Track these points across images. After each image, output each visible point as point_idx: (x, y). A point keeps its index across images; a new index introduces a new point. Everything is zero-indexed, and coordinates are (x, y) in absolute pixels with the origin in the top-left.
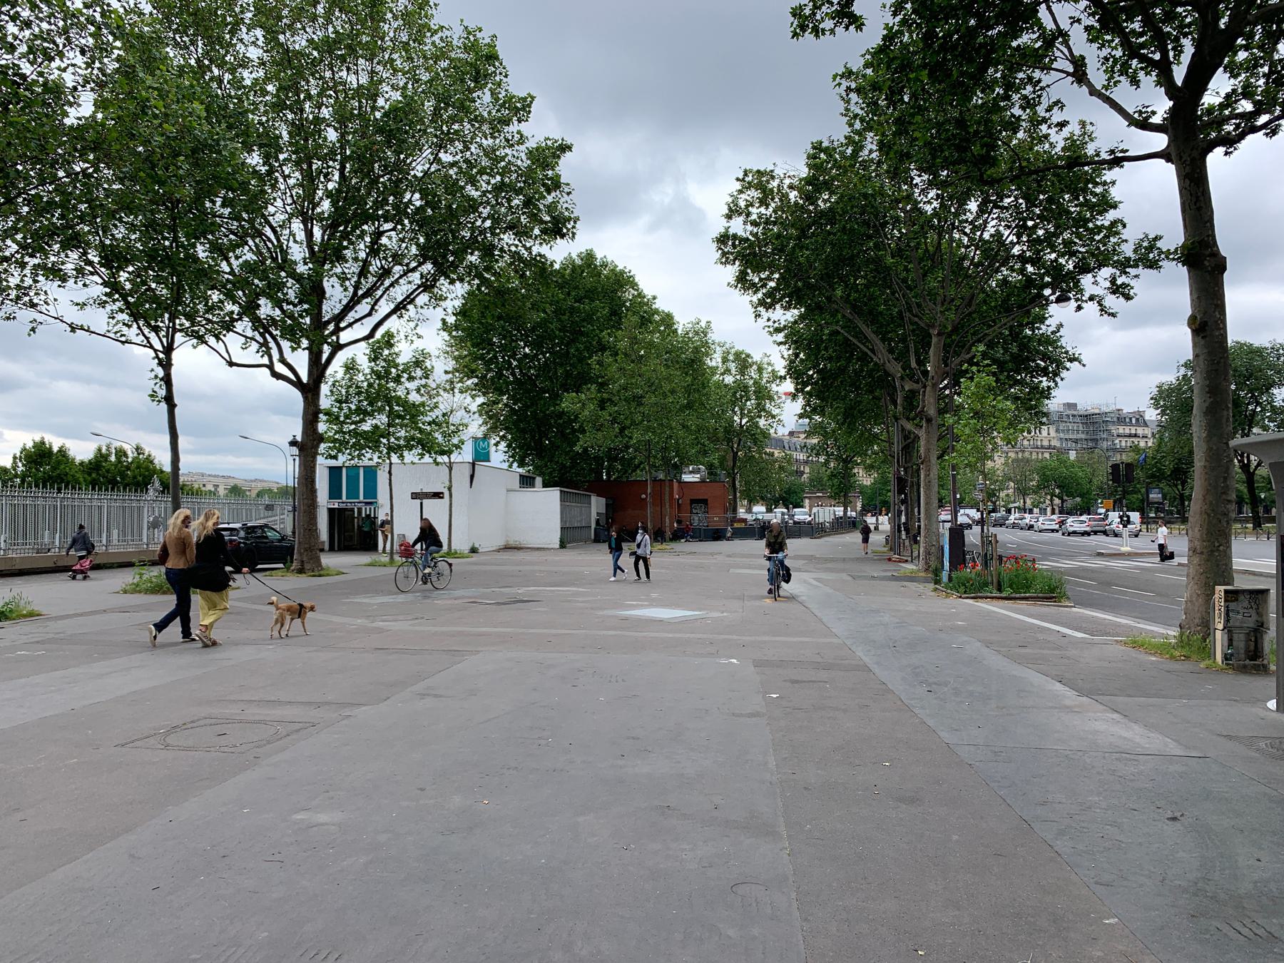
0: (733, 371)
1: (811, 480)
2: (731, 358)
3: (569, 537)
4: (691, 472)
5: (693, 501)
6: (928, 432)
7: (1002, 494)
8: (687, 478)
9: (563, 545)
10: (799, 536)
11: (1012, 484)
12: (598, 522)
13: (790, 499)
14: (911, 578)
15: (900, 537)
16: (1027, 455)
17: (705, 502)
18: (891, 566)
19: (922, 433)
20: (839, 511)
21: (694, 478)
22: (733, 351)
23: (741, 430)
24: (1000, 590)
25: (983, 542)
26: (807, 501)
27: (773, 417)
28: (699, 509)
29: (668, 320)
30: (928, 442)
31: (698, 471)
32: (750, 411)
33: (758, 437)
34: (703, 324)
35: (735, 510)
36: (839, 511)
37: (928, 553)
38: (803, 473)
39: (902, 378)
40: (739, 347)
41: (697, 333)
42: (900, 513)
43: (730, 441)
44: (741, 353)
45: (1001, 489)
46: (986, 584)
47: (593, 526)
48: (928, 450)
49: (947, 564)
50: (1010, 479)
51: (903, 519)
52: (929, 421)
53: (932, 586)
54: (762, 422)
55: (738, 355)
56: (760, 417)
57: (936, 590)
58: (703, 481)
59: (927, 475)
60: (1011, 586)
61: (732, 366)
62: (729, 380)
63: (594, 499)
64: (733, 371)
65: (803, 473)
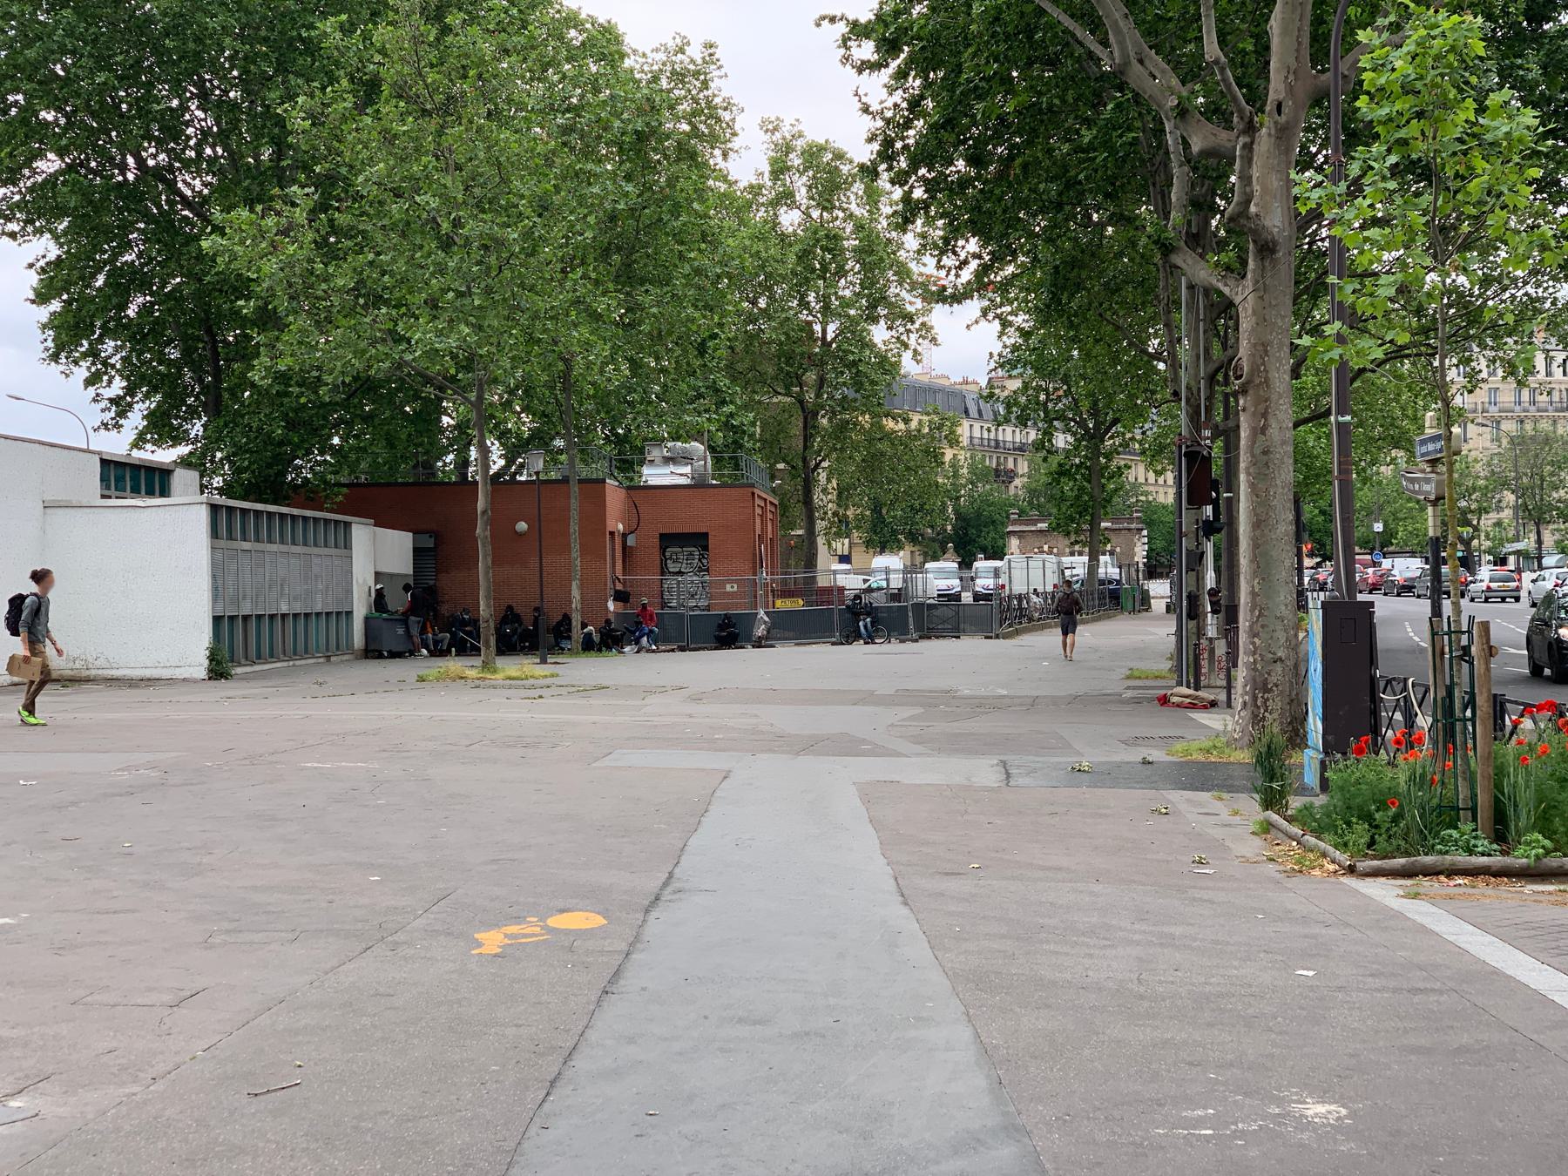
0: (801, 195)
1: (1032, 492)
2: (795, 160)
3: (240, 644)
4: (668, 460)
5: (667, 540)
6: (1261, 289)
7: (1487, 522)
8: (656, 475)
9: (218, 669)
10: (956, 632)
11: (1510, 498)
12: (379, 601)
13: (973, 538)
14: (1201, 776)
15: (1200, 632)
16: (1545, 425)
17: (700, 540)
18: (1162, 723)
19: (1243, 294)
20: (1078, 565)
21: (677, 476)
22: (799, 144)
23: (828, 355)
24: (1501, 835)
25: (1438, 653)
26: (1014, 543)
27: (910, 318)
28: (683, 559)
29: (605, 45)
30: (1262, 320)
31: (686, 458)
32: (846, 303)
33: (871, 378)
34: (695, 52)
35: (810, 562)
36: (1078, 565)
37: (1260, 686)
38: (1011, 475)
39: (1182, 112)
40: (815, 135)
41: (679, 77)
42: (1197, 558)
43: (791, 380)
44: (822, 149)
45: (1482, 511)
46: (1448, 814)
47: (360, 609)
48: (1262, 349)
49: (1315, 726)
50: (1505, 484)
51: (1210, 579)
52: (1267, 249)
53: (1250, 806)
54: (879, 334)
55: (813, 154)
56: (874, 320)
57: (1267, 828)
58: (699, 485)
59: (1260, 431)
60: (1544, 824)
61: (800, 186)
62: (789, 219)
63: (362, 534)
64: (801, 195)
65: (1011, 475)
